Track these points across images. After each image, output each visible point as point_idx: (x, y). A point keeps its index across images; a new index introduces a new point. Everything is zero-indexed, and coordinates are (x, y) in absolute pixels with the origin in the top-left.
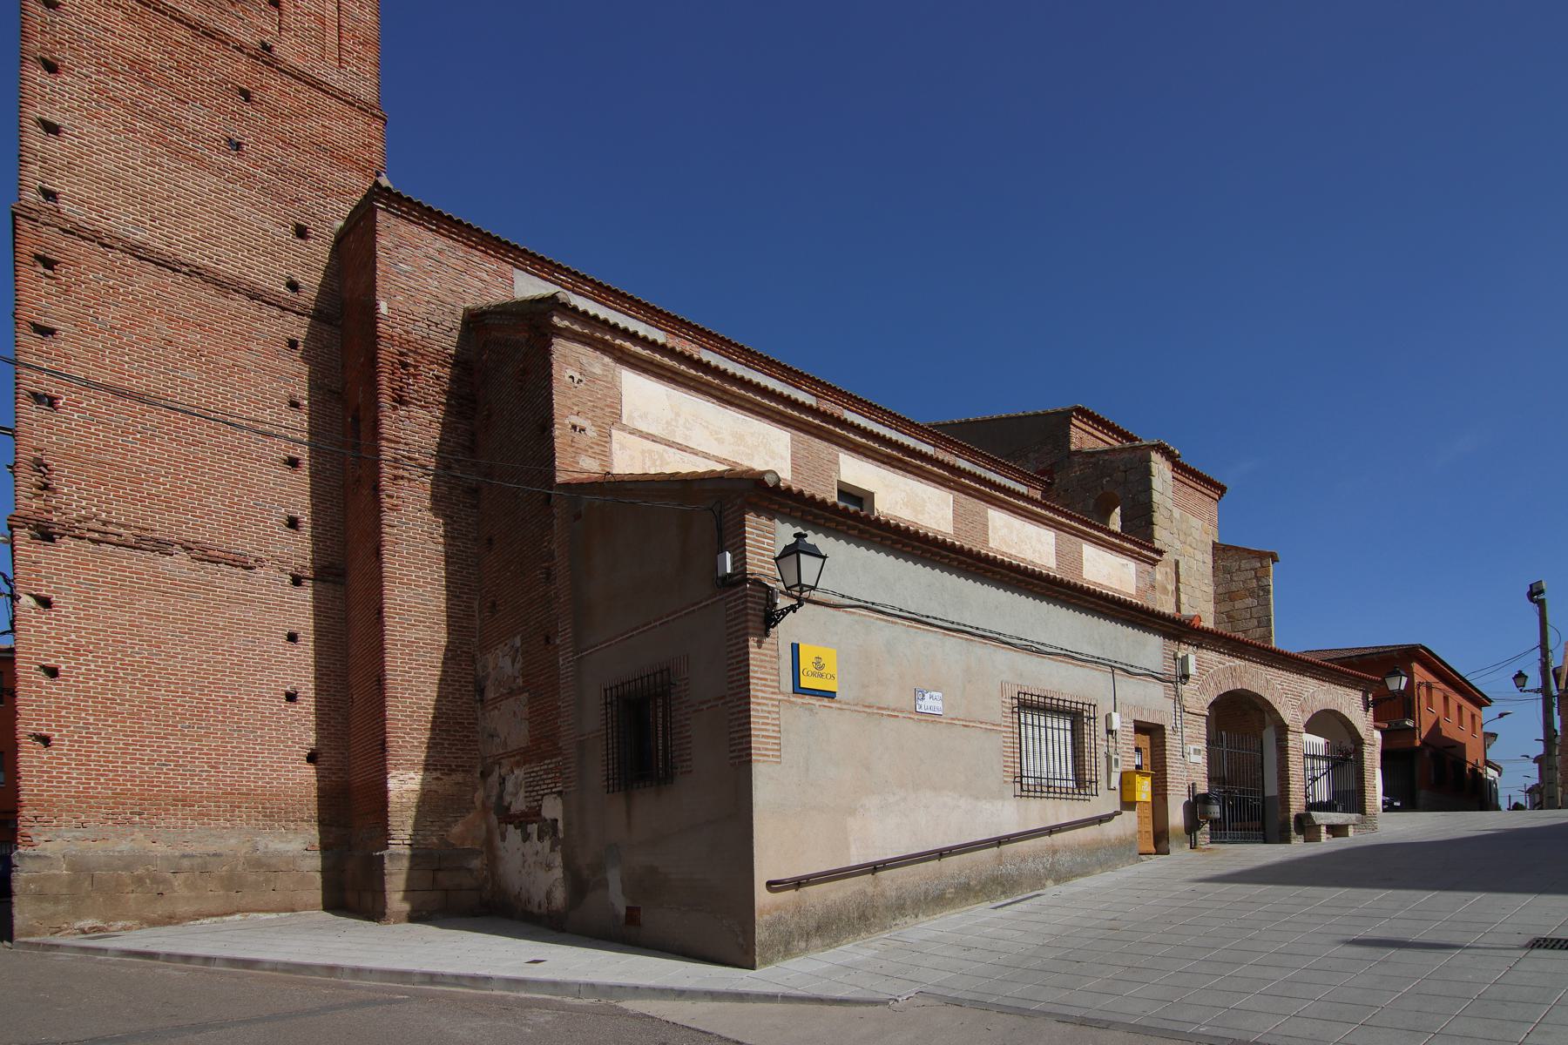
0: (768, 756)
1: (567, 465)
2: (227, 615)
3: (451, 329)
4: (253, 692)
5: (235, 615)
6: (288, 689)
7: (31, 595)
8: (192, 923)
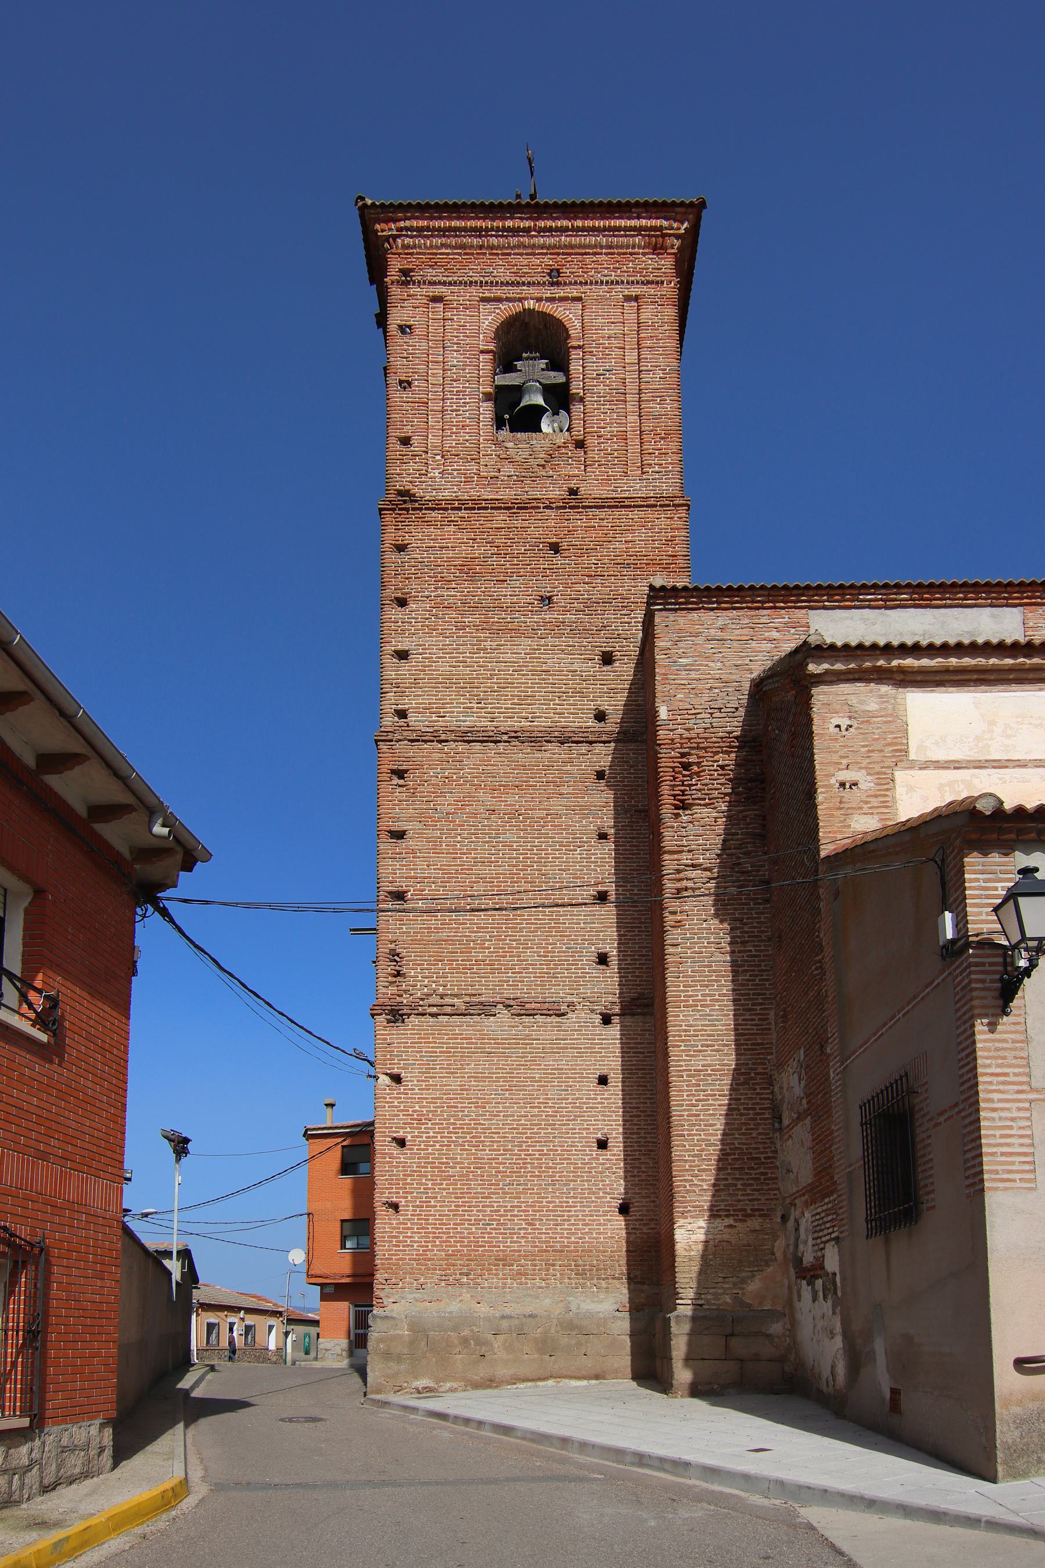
0: (1014, 1181)
1: (835, 832)
2: (543, 1067)
3: (737, 709)
4: (566, 1142)
5: (549, 1065)
6: (599, 1136)
7: (387, 1074)
8: (509, 1387)
